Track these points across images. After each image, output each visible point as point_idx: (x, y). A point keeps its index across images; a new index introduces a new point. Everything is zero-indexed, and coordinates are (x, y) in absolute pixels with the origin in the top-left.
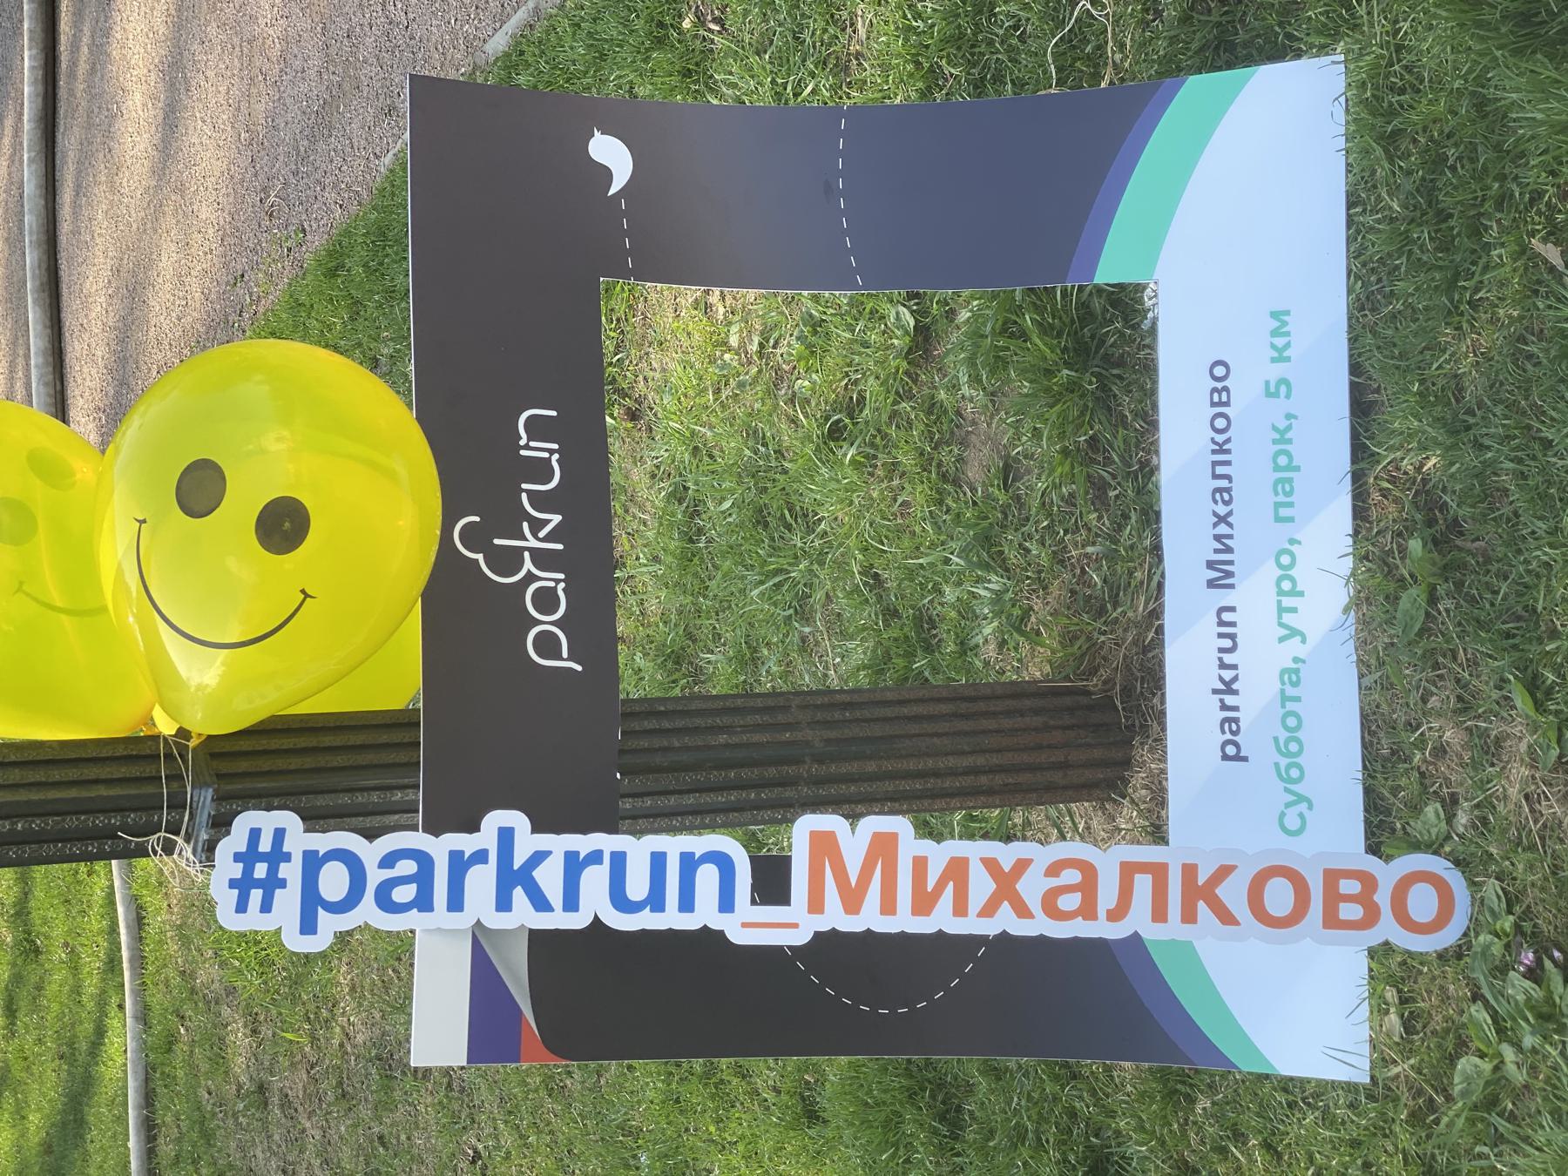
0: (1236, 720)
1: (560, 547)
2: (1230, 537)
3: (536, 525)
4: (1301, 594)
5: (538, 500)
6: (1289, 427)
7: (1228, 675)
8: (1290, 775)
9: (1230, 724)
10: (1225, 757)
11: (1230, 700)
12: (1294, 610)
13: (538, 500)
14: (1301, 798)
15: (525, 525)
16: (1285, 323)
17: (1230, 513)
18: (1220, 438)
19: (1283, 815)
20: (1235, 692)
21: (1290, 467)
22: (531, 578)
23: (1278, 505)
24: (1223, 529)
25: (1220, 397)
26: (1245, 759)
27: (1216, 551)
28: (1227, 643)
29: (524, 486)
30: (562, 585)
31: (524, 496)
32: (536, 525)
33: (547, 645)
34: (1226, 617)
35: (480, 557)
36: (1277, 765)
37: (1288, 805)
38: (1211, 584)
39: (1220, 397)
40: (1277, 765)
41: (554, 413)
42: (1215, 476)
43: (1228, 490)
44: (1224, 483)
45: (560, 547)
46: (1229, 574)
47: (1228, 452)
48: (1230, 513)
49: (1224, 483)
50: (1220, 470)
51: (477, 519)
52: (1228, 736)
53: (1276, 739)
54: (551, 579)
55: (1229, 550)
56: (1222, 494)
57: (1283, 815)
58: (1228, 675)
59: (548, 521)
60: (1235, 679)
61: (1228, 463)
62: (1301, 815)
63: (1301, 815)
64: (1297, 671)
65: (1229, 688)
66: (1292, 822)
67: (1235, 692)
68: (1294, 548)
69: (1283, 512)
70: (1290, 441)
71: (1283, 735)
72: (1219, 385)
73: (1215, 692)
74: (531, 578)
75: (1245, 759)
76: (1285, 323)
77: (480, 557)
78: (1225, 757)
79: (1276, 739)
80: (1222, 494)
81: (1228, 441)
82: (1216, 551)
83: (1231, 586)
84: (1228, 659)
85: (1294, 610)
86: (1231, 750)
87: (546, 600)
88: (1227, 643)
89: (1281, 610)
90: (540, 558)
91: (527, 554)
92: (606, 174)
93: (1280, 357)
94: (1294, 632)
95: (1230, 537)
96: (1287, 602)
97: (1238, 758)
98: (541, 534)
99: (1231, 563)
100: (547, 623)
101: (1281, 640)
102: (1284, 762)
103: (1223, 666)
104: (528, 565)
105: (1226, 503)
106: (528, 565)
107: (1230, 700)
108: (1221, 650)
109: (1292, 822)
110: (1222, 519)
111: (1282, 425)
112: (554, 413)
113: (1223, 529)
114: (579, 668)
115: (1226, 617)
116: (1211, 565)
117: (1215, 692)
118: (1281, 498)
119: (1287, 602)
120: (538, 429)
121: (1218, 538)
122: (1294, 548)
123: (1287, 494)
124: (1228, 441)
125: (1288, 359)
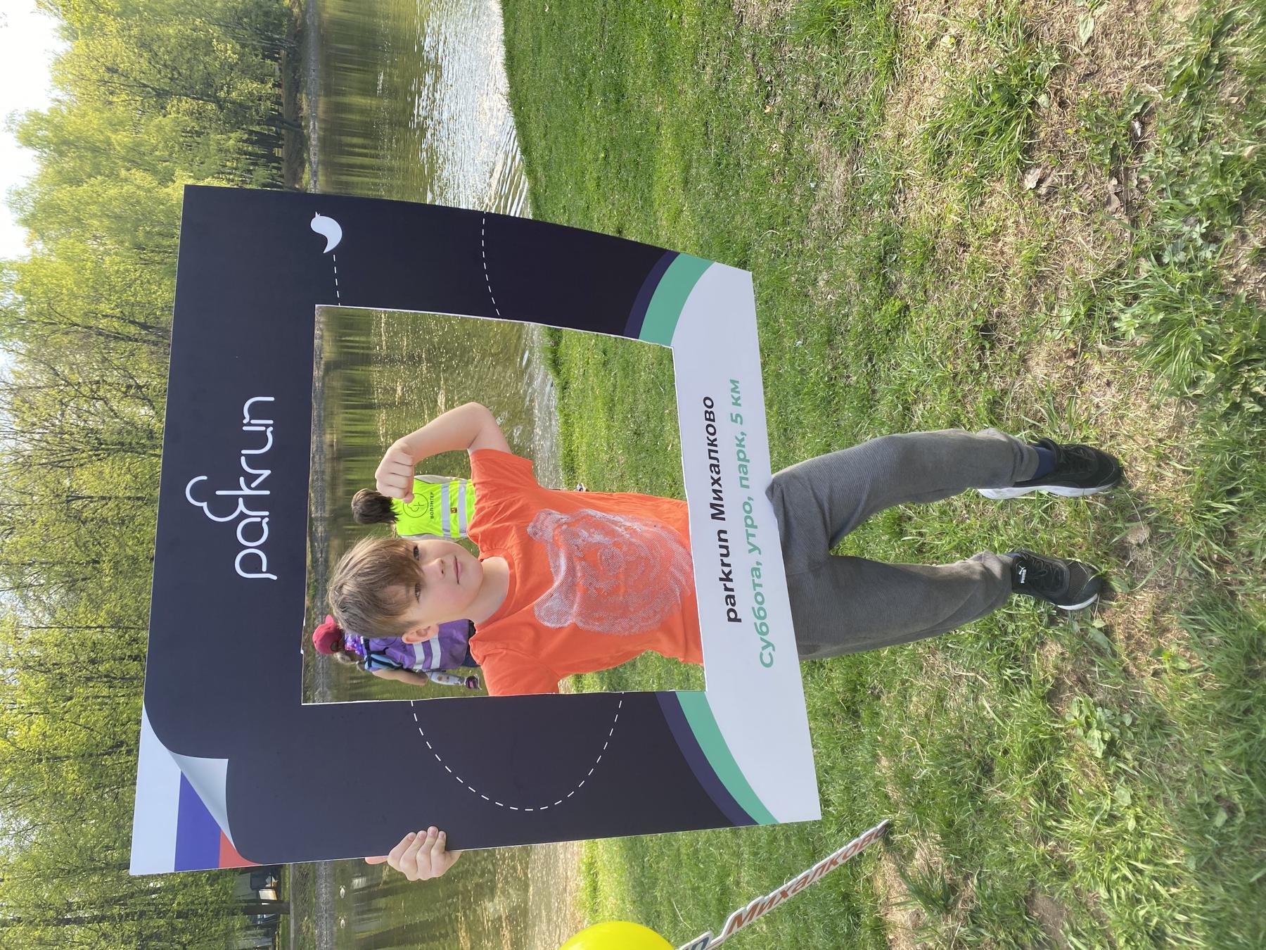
0: (733, 597)
1: (267, 492)
2: (721, 492)
3: (250, 479)
4: (756, 527)
5: (253, 461)
6: (743, 439)
7: (727, 570)
8: (762, 631)
9: (730, 599)
10: (730, 619)
11: (729, 585)
12: (753, 536)
13: (253, 461)
14: (769, 644)
15: (242, 479)
16: (737, 387)
17: (719, 479)
18: (712, 438)
19: (761, 654)
20: (731, 580)
21: (744, 460)
22: (243, 516)
23: (741, 478)
24: (716, 487)
25: (710, 416)
26: (739, 620)
27: (715, 498)
28: (725, 551)
29: (244, 452)
30: (271, 429)
31: (243, 459)
32: (250, 479)
33: (251, 563)
34: (723, 536)
35: (204, 505)
36: (755, 624)
37: (764, 648)
38: (713, 516)
39: (710, 416)
40: (755, 624)
41: (272, 399)
42: (711, 458)
43: (718, 466)
44: (715, 462)
45: (267, 492)
46: (722, 512)
47: (716, 446)
48: (719, 479)
49: (715, 462)
50: (713, 454)
51: (205, 478)
52: (730, 606)
53: (753, 608)
54: (255, 516)
55: (720, 499)
56: (715, 467)
57: (761, 654)
58: (727, 570)
59: (259, 476)
60: (730, 572)
61: (716, 452)
62: (770, 654)
63: (770, 654)
64: (759, 569)
65: (727, 578)
66: (767, 660)
67: (731, 580)
68: (750, 502)
69: (744, 482)
70: (744, 446)
71: (757, 606)
72: (709, 410)
73: (721, 579)
74: (243, 516)
75: (739, 620)
76: (737, 387)
77: (204, 505)
78: (730, 619)
79: (753, 608)
80: (715, 467)
81: (715, 440)
82: (715, 498)
83: (724, 519)
84: (726, 560)
85: (753, 536)
86: (732, 615)
87: (253, 532)
88: (725, 551)
89: (749, 535)
90: (252, 502)
91: (241, 500)
92: (323, 240)
93: (736, 403)
94: (755, 548)
95: (721, 492)
96: (751, 531)
97: (737, 620)
98: (253, 485)
99: (722, 506)
100: (252, 547)
101: (750, 551)
102: (759, 622)
103: (724, 564)
104: (241, 507)
105: (718, 473)
106: (241, 507)
107: (729, 585)
108: (722, 555)
109: (767, 660)
110: (716, 482)
111: (740, 437)
112: (272, 399)
113: (716, 487)
114: (275, 578)
115: (723, 536)
116: (712, 506)
117: (721, 579)
118: (742, 475)
119: (751, 531)
120: (257, 411)
121: (715, 491)
122: (750, 502)
123: (746, 473)
124: (715, 440)
125: (740, 405)
